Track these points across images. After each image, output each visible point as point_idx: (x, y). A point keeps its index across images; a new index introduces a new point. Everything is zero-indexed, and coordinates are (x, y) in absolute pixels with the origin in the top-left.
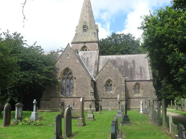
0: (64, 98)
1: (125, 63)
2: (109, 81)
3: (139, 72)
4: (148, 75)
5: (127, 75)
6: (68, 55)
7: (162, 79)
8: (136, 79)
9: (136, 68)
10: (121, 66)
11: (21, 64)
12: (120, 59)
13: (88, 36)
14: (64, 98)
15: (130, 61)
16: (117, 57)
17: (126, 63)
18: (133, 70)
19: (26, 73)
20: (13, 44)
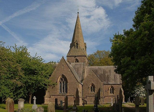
0: (60, 96)
1: (104, 71)
2: (93, 85)
3: (113, 78)
4: (33, 52)
5: (105, 81)
6: (63, 65)
7: (136, 86)
8: (111, 83)
9: (111, 76)
10: (102, 74)
11: (25, 70)
12: (100, 69)
13: (78, 51)
14: (60, 96)
15: (107, 70)
16: (99, 68)
17: (105, 72)
18: (109, 77)
19: (31, 77)
20: (3, 49)
